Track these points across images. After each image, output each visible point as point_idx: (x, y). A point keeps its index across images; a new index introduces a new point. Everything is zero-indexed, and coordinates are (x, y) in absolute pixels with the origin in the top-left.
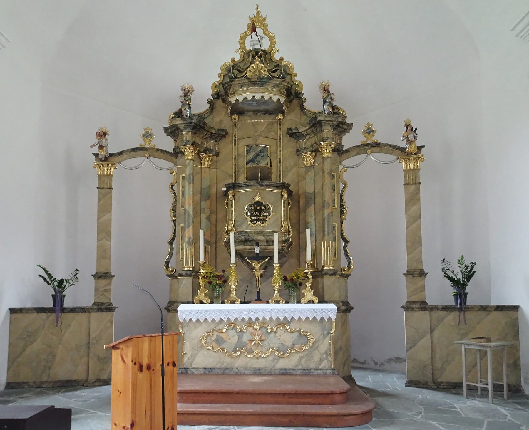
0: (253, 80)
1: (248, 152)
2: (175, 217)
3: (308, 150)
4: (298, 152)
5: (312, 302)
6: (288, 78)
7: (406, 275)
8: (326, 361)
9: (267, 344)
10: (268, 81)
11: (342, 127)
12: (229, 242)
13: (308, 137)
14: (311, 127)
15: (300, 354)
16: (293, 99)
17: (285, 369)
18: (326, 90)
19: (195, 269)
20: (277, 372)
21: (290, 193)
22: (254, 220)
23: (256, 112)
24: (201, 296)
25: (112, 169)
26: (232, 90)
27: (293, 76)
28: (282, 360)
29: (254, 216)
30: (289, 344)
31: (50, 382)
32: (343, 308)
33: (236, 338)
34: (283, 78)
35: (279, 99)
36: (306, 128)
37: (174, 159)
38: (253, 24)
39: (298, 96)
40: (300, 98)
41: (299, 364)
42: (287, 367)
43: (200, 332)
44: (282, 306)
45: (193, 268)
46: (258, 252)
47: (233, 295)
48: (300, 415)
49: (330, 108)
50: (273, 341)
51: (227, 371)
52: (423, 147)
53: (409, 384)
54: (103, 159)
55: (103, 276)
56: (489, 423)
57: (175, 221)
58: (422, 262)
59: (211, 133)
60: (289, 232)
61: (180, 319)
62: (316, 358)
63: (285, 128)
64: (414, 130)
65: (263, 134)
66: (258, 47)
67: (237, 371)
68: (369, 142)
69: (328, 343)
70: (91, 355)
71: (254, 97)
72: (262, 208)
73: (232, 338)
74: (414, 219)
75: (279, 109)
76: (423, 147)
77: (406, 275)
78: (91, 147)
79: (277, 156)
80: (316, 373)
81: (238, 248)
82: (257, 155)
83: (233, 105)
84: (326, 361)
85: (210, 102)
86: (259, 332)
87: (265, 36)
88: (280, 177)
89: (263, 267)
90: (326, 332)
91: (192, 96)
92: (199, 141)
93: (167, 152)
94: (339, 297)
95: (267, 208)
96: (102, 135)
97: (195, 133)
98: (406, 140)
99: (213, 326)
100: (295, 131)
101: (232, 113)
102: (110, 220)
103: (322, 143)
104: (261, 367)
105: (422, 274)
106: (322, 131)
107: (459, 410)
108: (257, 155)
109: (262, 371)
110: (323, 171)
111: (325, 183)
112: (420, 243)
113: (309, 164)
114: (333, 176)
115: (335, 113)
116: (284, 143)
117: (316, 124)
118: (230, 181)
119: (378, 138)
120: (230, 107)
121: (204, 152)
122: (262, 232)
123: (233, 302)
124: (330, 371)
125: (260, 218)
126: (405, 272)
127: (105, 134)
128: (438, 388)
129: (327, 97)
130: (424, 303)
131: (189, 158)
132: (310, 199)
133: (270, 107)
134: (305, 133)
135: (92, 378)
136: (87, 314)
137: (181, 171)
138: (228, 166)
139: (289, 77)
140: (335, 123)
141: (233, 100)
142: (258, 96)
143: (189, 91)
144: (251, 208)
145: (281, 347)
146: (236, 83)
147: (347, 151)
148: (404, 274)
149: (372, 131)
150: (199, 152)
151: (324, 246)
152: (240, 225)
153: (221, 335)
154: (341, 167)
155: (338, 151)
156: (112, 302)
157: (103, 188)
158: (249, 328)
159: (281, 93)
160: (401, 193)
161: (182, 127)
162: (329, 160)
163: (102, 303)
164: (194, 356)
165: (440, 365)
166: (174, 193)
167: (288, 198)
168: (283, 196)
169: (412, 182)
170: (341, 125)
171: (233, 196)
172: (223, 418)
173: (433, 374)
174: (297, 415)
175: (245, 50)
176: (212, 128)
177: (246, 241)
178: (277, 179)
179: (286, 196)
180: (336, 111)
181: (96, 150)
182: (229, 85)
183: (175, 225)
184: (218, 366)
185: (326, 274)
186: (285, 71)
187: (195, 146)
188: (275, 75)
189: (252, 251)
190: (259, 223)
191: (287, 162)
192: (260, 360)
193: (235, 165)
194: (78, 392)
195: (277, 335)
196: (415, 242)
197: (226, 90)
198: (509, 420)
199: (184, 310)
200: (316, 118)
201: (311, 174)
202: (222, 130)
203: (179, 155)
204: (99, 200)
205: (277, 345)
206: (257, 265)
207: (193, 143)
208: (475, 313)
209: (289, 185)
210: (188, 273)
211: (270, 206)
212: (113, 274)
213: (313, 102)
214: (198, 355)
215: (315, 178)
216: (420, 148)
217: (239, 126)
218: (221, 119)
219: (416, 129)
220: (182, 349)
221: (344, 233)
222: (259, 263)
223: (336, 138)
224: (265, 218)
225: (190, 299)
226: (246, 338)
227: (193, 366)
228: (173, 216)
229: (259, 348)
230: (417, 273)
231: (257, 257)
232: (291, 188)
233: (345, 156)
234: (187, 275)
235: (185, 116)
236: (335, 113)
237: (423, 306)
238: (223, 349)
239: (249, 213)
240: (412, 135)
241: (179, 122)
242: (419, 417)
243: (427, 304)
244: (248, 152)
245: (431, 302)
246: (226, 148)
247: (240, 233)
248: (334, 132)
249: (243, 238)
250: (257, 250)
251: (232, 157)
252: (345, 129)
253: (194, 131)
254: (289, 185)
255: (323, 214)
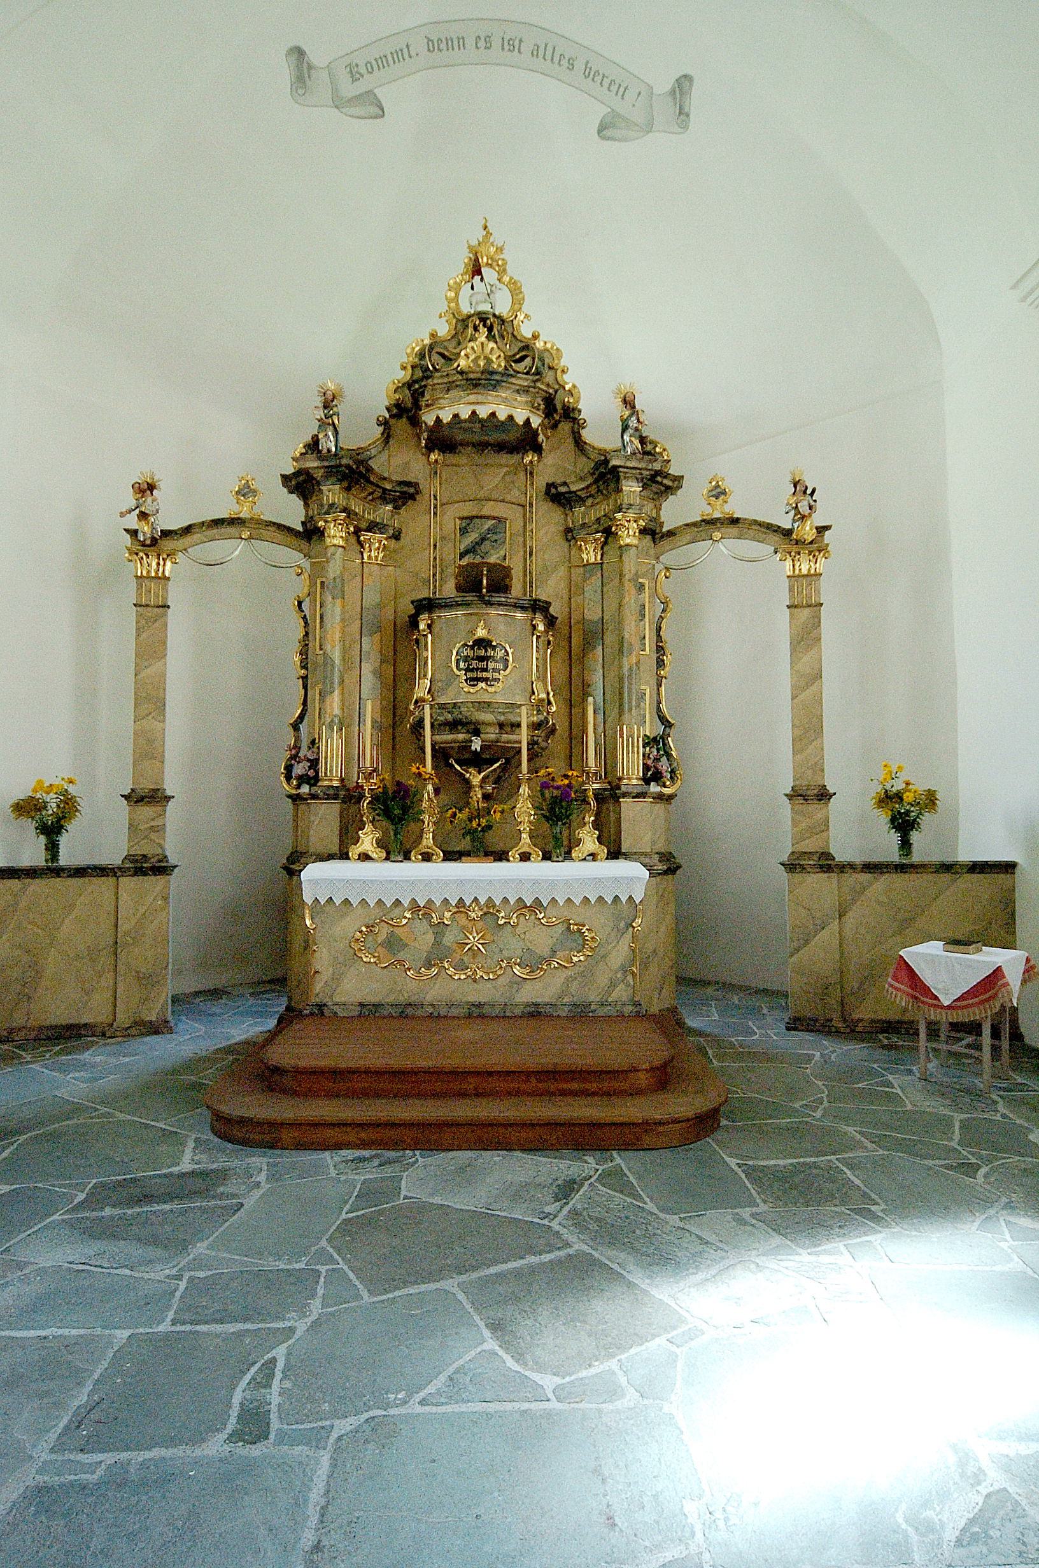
0: (472, 376)
1: (464, 531)
2: (307, 669)
3: (589, 530)
4: (569, 534)
5: (593, 856)
6: (549, 377)
7: (790, 797)
8: (622, 986)
9: (497, 950)
10: (504, 379)
11: (660, 483)
12: (420, 723)
13: (589, 502)
14: (596, 481)
15: (568, 973)
16: (560, 421)
17: (536, 1005)
18: (628, 402)
19: (346, 782)
20: (518, 1011)
21: (551, 621)
22: (472, 679)
23: (481, 446)
24: (367, 841)
25: (168, 563)
26: (427, 397)
27: (559, 372)
28: (528, 986)
29: (472, 670)
30: (546, 952)
31: (32, 1029)
32: (661, 867)
33: (430, 938)
34: (538, 373)
35: (528, 420)
36: (587, 483)
37: (304, 544)
38: (477, 260)
39: (570, 414)
40: (575, 420)
41: (564, 993)
42: (539, 1000)
43: (350, 926)
44: (538, 869)
45: (342, 780)
46: (479, 749)
47: (428, 840)
48: (562, 1125)
49: (637, 443)
50: (512, 945)
51: (409, 1010)
52: (827, 528)
53: (793, 1025)
54: (148, 542)
55: (147, 797)
56: (964, 1125)
57: (305, 678)
58: (823, 770)
59: (384, 490)
60: (549, 703)
61: (308, 898)
62: (602, 980)
63: (541, 482)
64: (809, 491)
65: (495, 495)
66: (485, 307)
67: (431, 1010)
68: (717, 515)
69: (626, 948)
70: (121, 968)
71: (474, 412)
72: (490, 653)
73: (422, 939)
74: (809, 680)
75: (527, 441)
76: (827, 528)
77: (790, 797)
78: (122, 515)
79: (525, 541)
80: (601, 1012)
81: (437, 738)
82: (483, 539)
83: (431, 430)
84: (622, 986)
85: (384, 423)
86: (480, 925)
87: (500, 286)
88: (531, 586)
89: (492, 779)
90: (622, 925)
91: (340, 409)
92: (357, 507)
93: (289, 530)
94: (654, 843)
95: (500, 653)
96: (147, 488)
97: (348, 489)
98: (793, 512)
99: (378, 912)
100: (562, 489)
101: (430, 448)
102: (163, 675)
103: (619, 516)
104: (483, 1000)
105: (824, 796)
106: (619, 490)
107: (899, 1091)
108: (483, 539)
109: (486, 1010)
110: (621, 576)
111: (625, 601)
112: (819, 732)
113: (592, 560)
114: (643, 585)
115: (646, 453)
116: (540, 514)
117: (606, 475)
118: (424, 594)
119: (735, 507)
120: (425, 435)
121: (369, 530)
122: (489, 704)
123: (427, 857)
124: (631, 1008)
125: (485, 675)
126: (788, 791)
127: (151, 487)
128: (852, 1031)
129: (631, 416)
130: (826, 855)
131: (335, 542)
132: (592, 635)
133: (512, 436)
134: (583, 494)
135: (123, 1019)
136: (112, 880)
137: (318, 569)
138: (420, 563)
139: (551, 373)
140: (646, 473)
141: (429, 418)
142: (483, 412)
143: (334, 397)
144: (468, 652)
145: (527, 956)
146: (436, 381)
147: (670, 533)
148: (786, 795)
149: (724, 493)
150: (357, 531)
151: (622, 736)
152: (443, 690)
153: (397, 930)
154: (659, 567)
155: (653, 532)
156: (167, 854)
157: (147, 606)
158: (457, 916)
159: (534, 408)
160: (782, 625)
161: (318, 475)
162: (633, 551)
163: (144, 856)
164: (337, 978)
165: (856, 985)
166: (304, 618)
167: (546, 631)
168: (534, 627)
169: (805, 605)
170: (659, 479)
171: (429, 626)
172: (388, 1133)
173: (842, 1004)
174: (552, 1125)
175: (459, 312)
176: (385, 479)
177: (454, 725)
178: (525, 591)
179: (541, 627)
180: (649, 448)
181: (132, 521)
182: (421, 387)
183: (305, 687)
184: (390, 1000)
185: (625, 795)
186: (542, 360)
187: (348, 517)
188: (520, 367)
189: (465, 747)
190: (483, 685)
191: (539, 553)
192: (481, 986)
193: (435, 558)
194: (86, 1056)
195: (519, 930)
196: (809, 729)
197: (417, 395)
198: (1004, 1116)
199: (317, 877)
200: (606, 462)
201: (596, 580)
202: (409, 484)
203: (315, 538)
204: (139, 631)
205: (519, 953)
206: (476, 778)
207: (345, 510)
208: (931, 877)
209: (549, 604)
210: (331, 792)
211: (508, 648)
212: (169, 793)
213: (601, 428)
214: (343, 976)
215: (605, 590)
216: (822, 530)
217: (444, 478)
218: (402, 462)
219: (814, 491)
220: (308, 963)
221: (663, 706)
222: (479, 773)
223: (649, 507)
224: (496, 675)
225: (335, 849)
226: (449, 939)
227: (337, 999)
228: (302, 668)
229: (479, 959)
230: (812, 795)
231: (477, 761)
232: (551, 610)
233: (666, 543)
234: (328, 797)
235: (325, 451)
236: (646, 453)
237: (826, 864)
238: (401, 962)
239: (462, 665)
240: (806, 503)
241: (312, 463)
242: (818, 1114)
243: (834, 859)
244: (464, 531)
245: (841, 855)
246: (414, 521)
247: (442, 707)
248: (644, 493)
249: (449, 717)
250: (476, 745)
251: (429, 545)
252: (668, 488)
253: (345, 484)
254: (549, 604)
255: (620, 667)
